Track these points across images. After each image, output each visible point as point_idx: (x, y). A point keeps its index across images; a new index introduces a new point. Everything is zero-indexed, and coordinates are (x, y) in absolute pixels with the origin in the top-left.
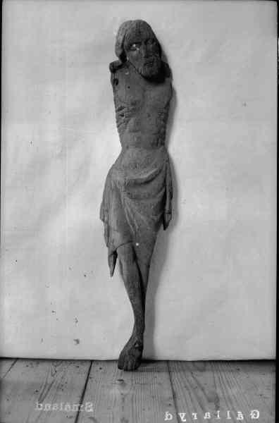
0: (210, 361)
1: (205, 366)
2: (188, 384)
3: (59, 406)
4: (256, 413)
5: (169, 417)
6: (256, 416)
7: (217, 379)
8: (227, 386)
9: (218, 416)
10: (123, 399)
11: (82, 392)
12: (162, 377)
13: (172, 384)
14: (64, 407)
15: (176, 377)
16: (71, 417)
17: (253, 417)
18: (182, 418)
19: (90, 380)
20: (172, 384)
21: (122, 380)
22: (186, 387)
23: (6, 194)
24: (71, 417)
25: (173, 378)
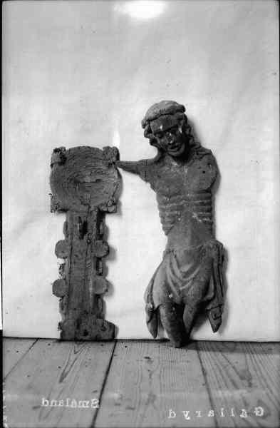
0: (241, 342)
1: (236, 345)
2: (217, 362)
3: (65, 403)
4: (259, 410)
5: (173, 415)
6: (260, 413)
7: (249, 361)
8: (260, 365)
9: (222, 413)
10: (150, 375)
11: (112, 364)
12: (193, 353)
13: (201, 362)
14: (70, 403)
15: (204, 355)
16: (95, 392)
17: (257, 414)
18: (186, 416)
19: (114, 357)
20: (201, 362)
21: (149, 358)
22: (216, 365)
23: (6, 384)
24: (95, 392)
25: (202, 357)
